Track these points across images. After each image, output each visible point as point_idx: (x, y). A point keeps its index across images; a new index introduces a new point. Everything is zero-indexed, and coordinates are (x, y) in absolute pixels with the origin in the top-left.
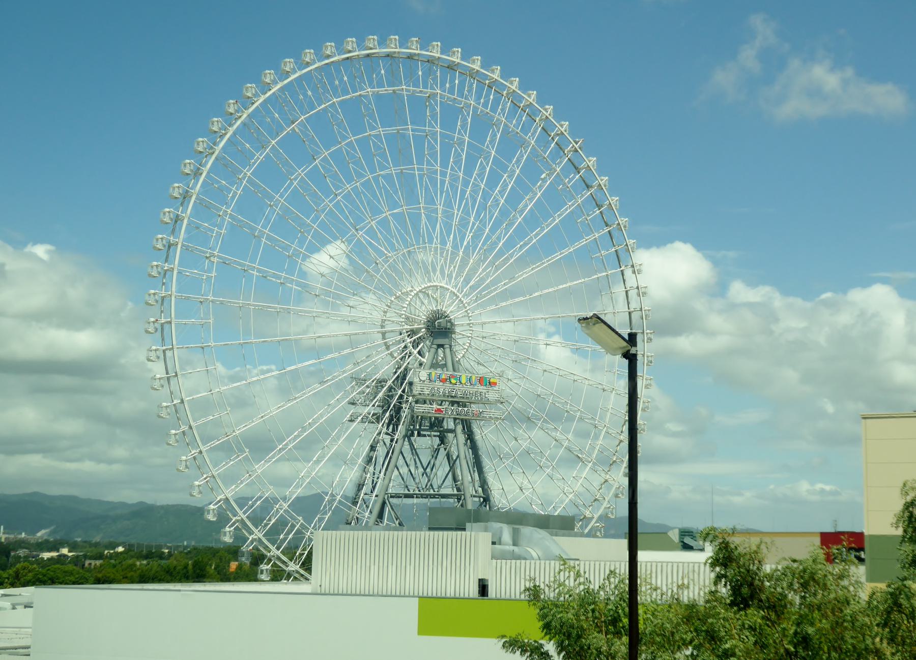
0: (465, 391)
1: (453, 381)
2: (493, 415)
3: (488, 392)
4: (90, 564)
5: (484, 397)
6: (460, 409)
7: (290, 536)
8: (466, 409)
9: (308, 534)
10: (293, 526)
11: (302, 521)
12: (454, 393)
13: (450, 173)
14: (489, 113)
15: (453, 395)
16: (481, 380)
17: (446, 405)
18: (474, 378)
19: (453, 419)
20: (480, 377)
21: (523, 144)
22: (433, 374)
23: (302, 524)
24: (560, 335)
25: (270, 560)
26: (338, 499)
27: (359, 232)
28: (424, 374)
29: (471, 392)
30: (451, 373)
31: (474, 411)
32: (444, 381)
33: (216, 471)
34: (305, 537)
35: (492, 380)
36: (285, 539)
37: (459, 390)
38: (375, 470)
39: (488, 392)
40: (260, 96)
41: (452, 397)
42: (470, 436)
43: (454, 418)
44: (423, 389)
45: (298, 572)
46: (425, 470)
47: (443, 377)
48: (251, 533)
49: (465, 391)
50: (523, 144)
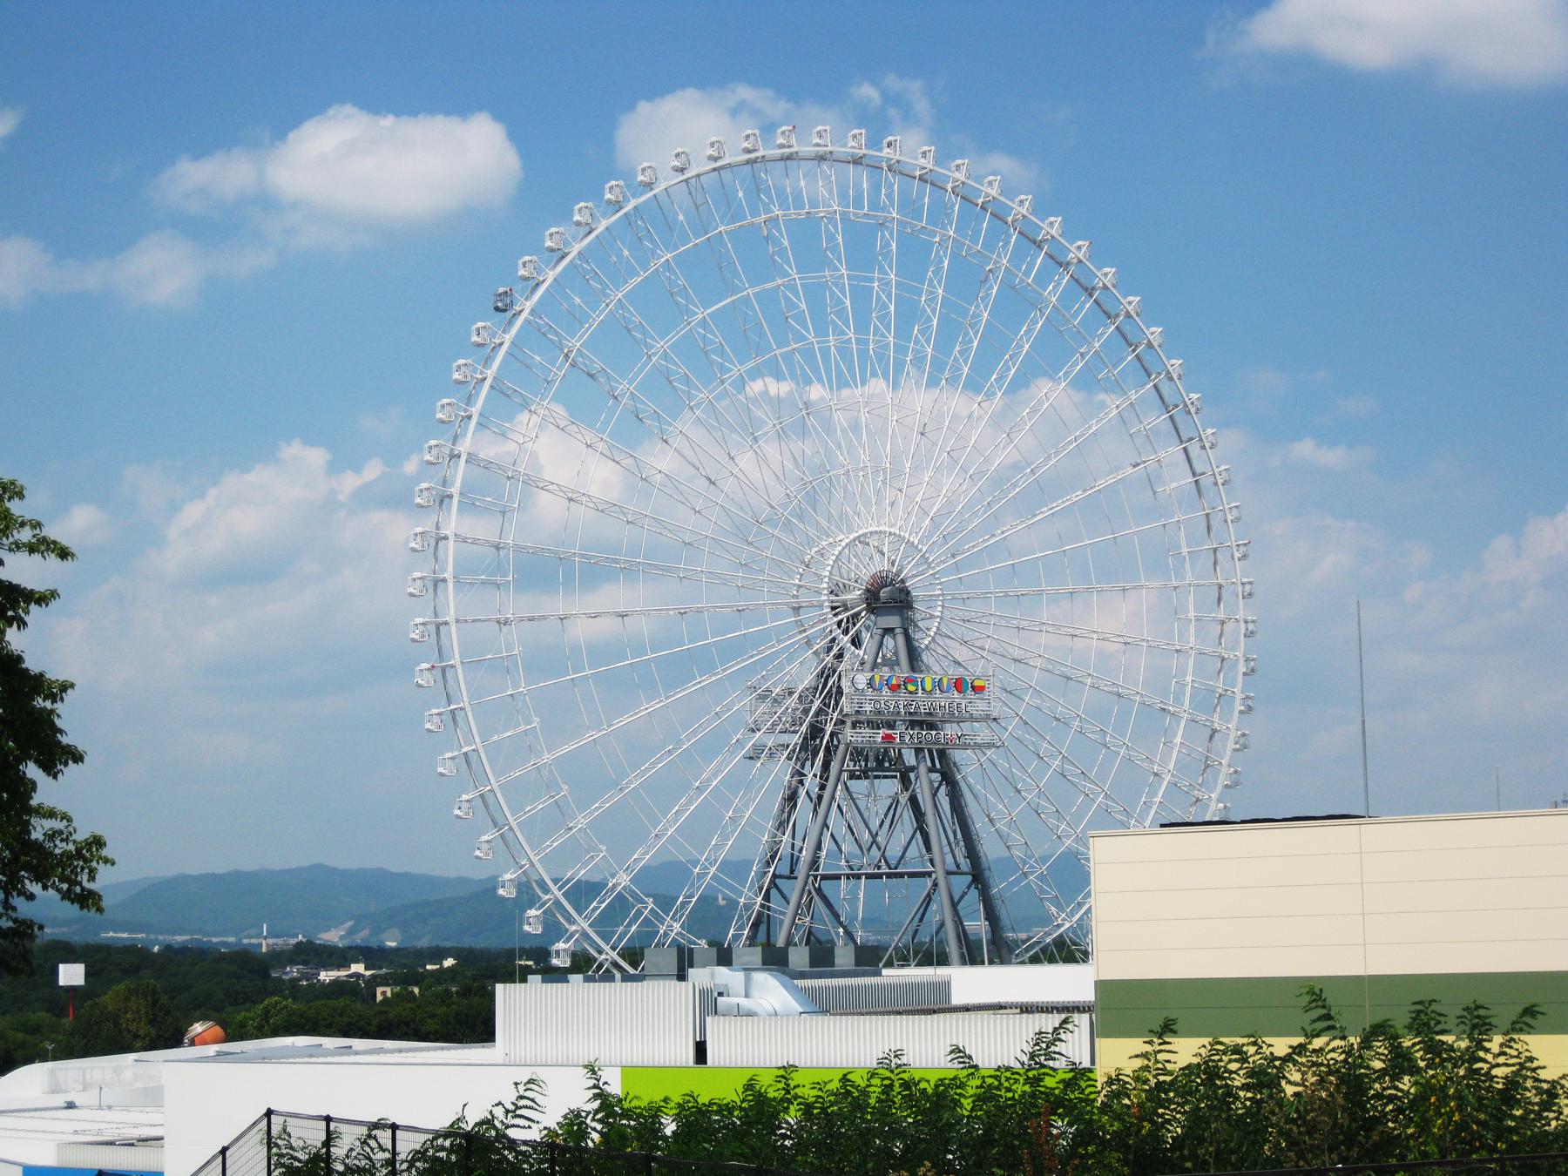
0: (932, 704)
1: (911, 688)
2: (972, 739)
3: (970, 703)
4: (384, 993)
5: (964, 711)
6: (924, 733)
7: (634, 928)
8: (934, 733)
9: (664, 928)
10: (639, 912)
11: (651, 906)
12: (913, 707)
13: (873, 340)
14: (925, 228)
15: (912, 711)
16: (959, 685)
17: (900, 728)
18: (945, 681)
19: (913, 750)
20: (956, 679)
21: (1037, 304)
22: (877, 678)
23: (652, 910)
24: (786, 380)
25: (572, 936)
26: (712, 873)
27: (695, 411)
28: (862, 680)
29: (943, 704)
30: (906, 675)
31: (947, 735)
32: (894, 688)
33: (515, 820)
34: (659, 932)
35: (977, 683)
36: (625, 933)
37: (922, 704)
38: (793, 839)
39: (970, 703)
40: (573, 246)
41: (910, 713)
42: (948, 778)
43: (915, 748)
44: (862, 703)
45: (616, 965)
46: (874, 842)
47: (894, 682)
48: (571, 921)
49: (932, 704)
50: (1037, 304)
